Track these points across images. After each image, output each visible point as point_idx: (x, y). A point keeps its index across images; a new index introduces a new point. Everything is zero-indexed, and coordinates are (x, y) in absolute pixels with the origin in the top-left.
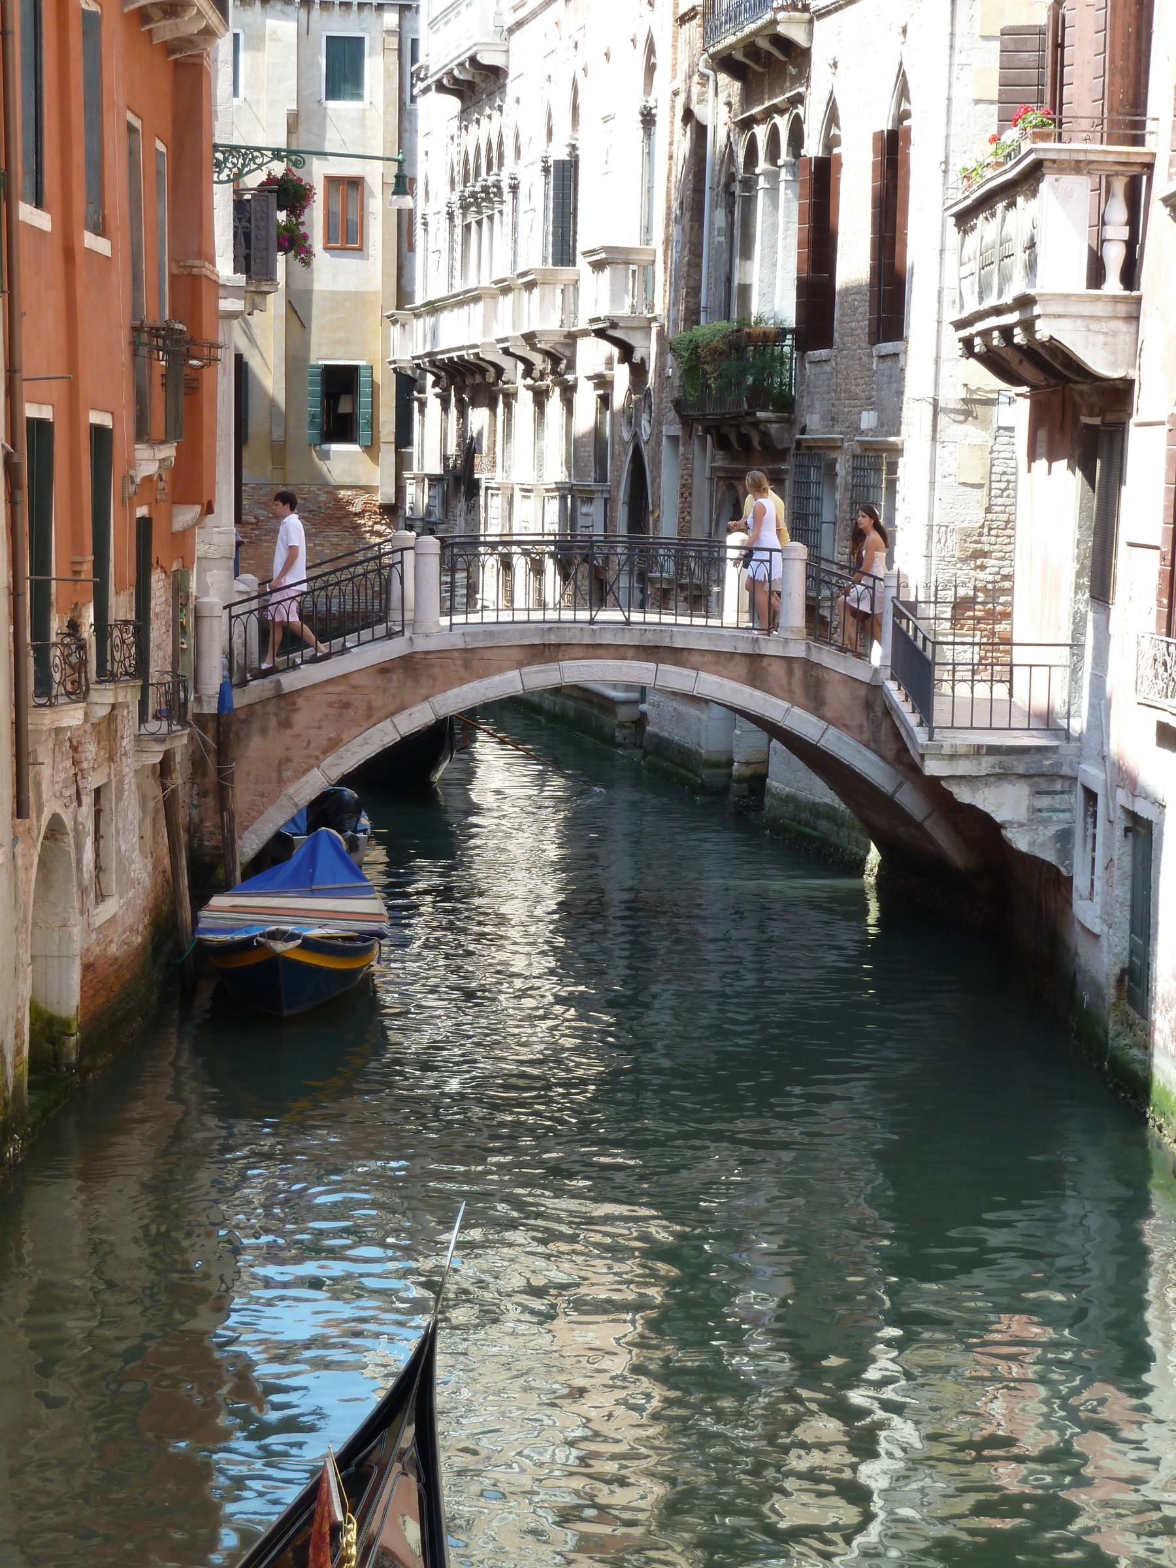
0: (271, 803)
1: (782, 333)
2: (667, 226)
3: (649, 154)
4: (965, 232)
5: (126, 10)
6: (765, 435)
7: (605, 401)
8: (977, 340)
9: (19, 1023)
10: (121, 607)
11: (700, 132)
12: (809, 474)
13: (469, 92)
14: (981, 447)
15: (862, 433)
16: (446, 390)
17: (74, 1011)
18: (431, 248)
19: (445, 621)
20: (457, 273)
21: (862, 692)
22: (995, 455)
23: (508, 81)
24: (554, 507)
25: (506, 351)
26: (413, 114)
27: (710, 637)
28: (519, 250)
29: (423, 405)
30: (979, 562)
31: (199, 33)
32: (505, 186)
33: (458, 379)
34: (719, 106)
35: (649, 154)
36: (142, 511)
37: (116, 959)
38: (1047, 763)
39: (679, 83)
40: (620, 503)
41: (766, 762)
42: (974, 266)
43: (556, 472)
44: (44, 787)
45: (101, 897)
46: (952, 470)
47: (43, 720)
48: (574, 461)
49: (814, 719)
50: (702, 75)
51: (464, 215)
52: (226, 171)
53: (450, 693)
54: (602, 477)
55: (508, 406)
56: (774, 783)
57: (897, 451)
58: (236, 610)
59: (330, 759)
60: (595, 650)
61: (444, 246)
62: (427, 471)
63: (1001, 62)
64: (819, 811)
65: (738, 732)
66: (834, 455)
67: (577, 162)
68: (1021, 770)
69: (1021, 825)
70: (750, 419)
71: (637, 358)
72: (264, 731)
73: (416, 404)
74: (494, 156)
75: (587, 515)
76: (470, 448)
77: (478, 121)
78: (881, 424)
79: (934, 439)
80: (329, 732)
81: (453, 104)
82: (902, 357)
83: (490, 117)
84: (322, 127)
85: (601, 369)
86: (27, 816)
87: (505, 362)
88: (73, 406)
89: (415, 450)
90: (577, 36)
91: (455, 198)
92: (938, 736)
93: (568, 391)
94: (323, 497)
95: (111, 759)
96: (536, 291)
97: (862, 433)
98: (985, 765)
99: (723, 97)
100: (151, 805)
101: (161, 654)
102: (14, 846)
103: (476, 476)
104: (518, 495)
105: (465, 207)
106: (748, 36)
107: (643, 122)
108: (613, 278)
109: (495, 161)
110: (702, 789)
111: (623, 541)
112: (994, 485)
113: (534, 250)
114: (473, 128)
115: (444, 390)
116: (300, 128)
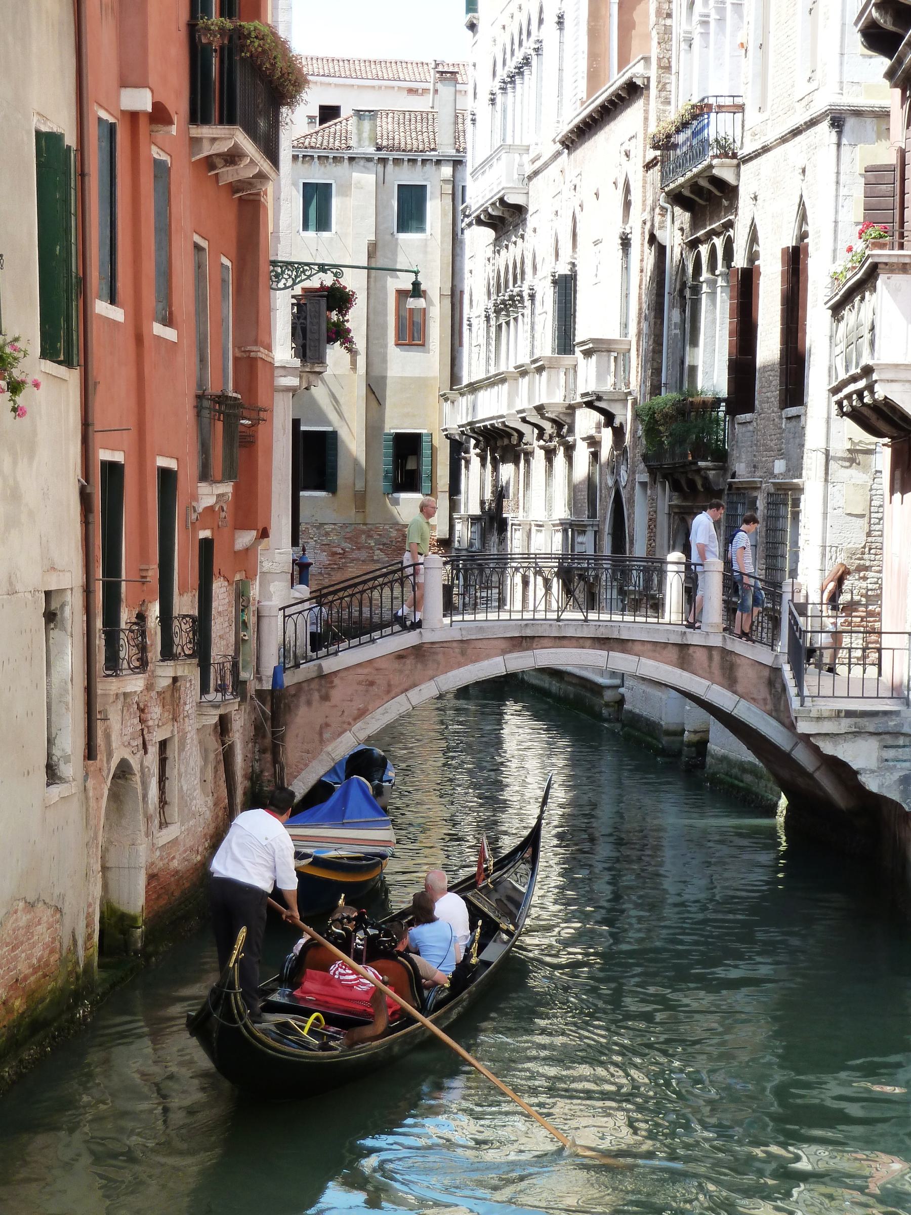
0: (314, 758)
1: (717, 402)
2: (639, 322)
3: (626, 269)
4: (839, 321)
5: (193, 159)
6: (706, 479)
7: (595, 456)
8: (845, 403)
9: (89, 916)
10: (185, 604)
11: (661, 252)
12: (737, 509)
13: (500, 225)
14: (863, 486)
15: (775, 477)
16: (484, 450)
17: (140, 909)
18: (474, 343)
19: (447, 621)
20: (492, 362)
21: (766, 673)
22: (873, 492)
23: (528, 216)
24: (559, 537)
25: (524, 420)
26: (462, 242)
27: (649, 631)
28: (535, 343)
29: (468, 462)
30: (862, 574)
31: (254, 177)
32: (526, 297)
33: (492, 442)
34: (674, 231)
35: (626, 269)
36: (205, 534)
37: (177, 872)
38: (892, 723)
39: (647, 216)
40: (606, 533)
41: (708, 731)
42: (842, 347)
43: (561, 512)
44: (114, 737)
45: (163, 824)
46: (841, 504)
47: (108, 687)
48: (573, 503)
49: (729, 694)
50: (662, 208)
51: (497, 318)
52: (283, 281)
53: (450, 674)
54: (593, 515)
55: (527, 462)
56: (713, 747)
57: (799, 490)
58: (288, 611)
59: (359, 724)
60: (561, 641)
61: (482, 341)
62: (470, 513)
63: (865, 192)
64: (744, 767)
65: (688, 708)
66: (755, 494)
67: (575, 275)
68: (872, 730)
69: (873, 772)
70: (694, 468)
71: (617, 423)
72: (309, 703)
73: (463, 462)
74: (518, 273)
75: (582, 543)
76: (500, 494)
77: (507, 247)
78: (788, 470)
79: (826, 480)
80: (358, 704)
81: (489, 234)
82: (803, 418)
83: (515, 243)
84: (395, 253)
85: (593, 432)
86: (95, 758)
87: (525, 429)
88: (141, 451)
89: (462, 497)
90: (576, 181)
91: (491, 305)
92: (808, 702)
93: (569, 449)
94: (394, 534)
95: (174, 719)
96: (544, 374)
97: (775, 477)
98: (844, 725)
99: (677, 224)
100: (212, 756)
101: (224, 642)
102: (85, 781)
103: (504, 516)
104: (534, 529)
105: (497, 312)
106: (692, 178)
107: (622, 244)
108: (598, 362)
109: (519, 277)
110: (663, 752)
111: (607, 565)
112: (873, 515)
113: (546, 345)
114: (503, 252)
115: (482, 450)
116: (378, 254)
